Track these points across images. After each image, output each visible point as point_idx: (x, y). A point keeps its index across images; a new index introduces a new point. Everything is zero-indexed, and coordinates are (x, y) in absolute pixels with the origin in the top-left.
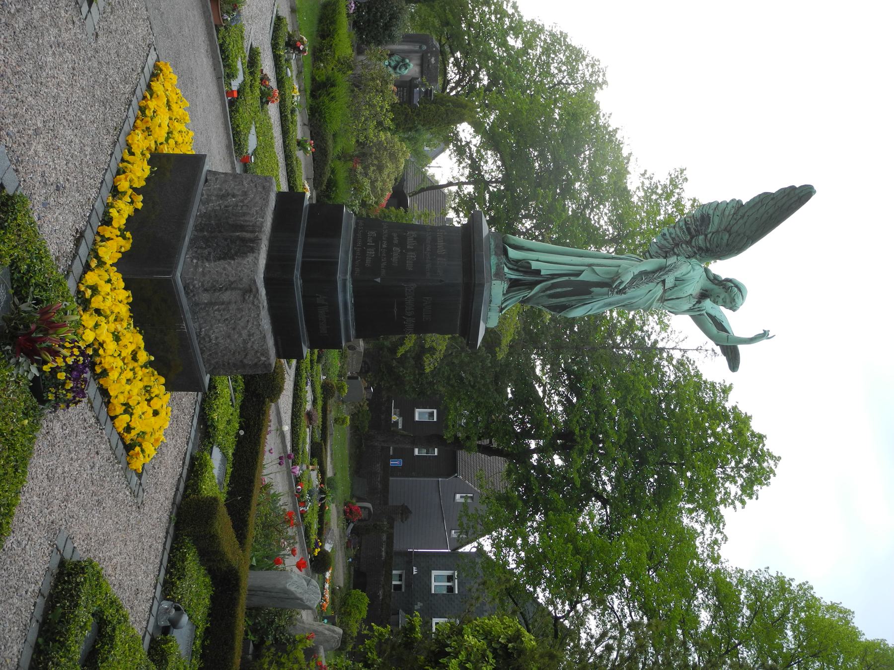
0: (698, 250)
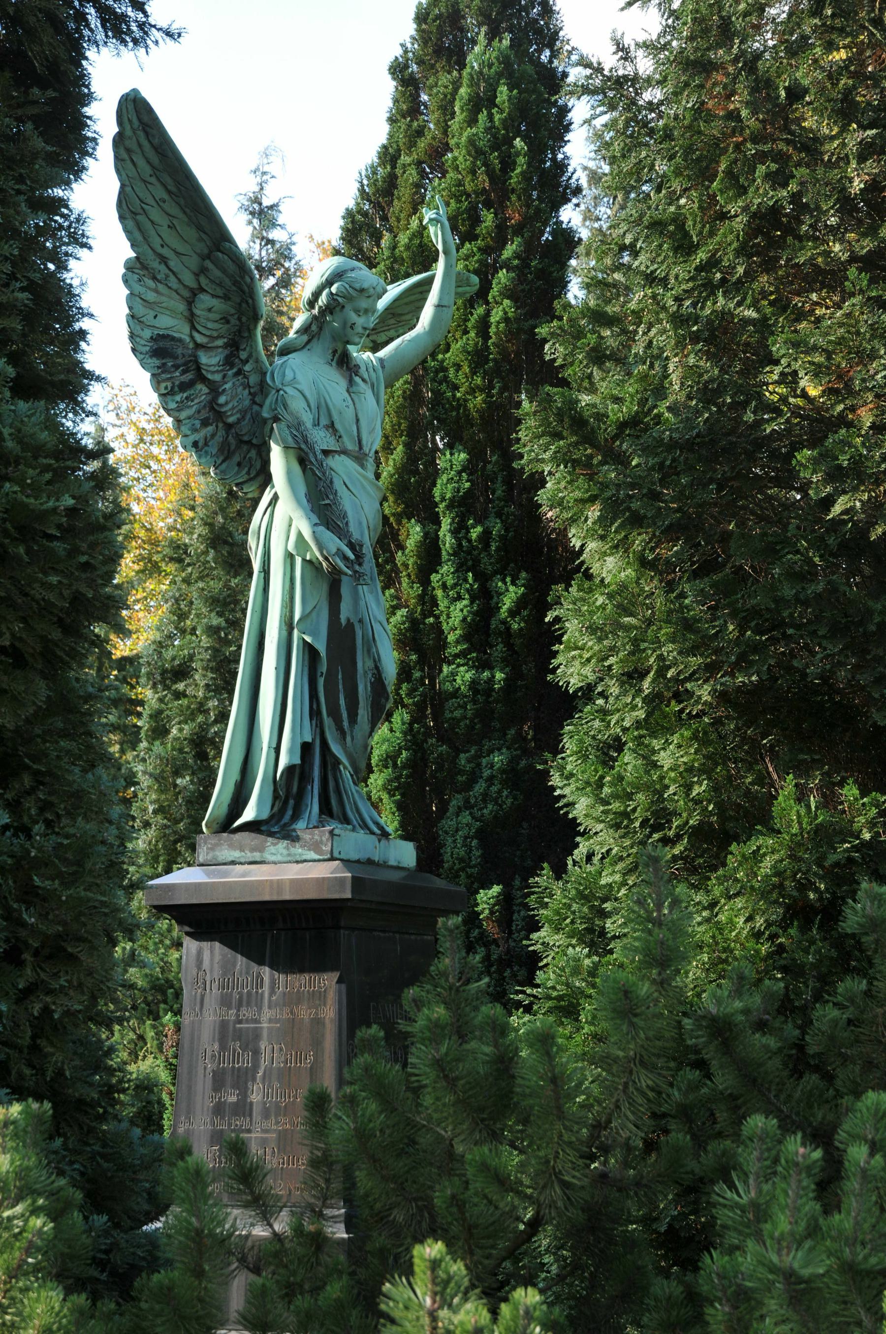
0: (232, 366)
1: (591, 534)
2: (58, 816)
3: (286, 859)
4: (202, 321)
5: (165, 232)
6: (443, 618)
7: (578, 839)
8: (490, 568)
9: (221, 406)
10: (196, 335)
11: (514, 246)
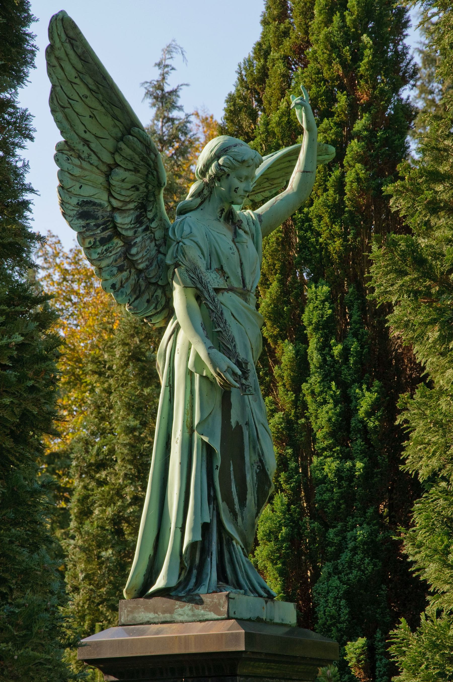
0: (141, 223)
1: (431, 351)
2: (11, 590)
3: (190, 619)
4: (117, 189)
5: (87, 121)
6: (312, 419)
7: (428, 598)
8: (349, 378)
9: (133, 255)
10: (112, 200)
11: (363, 121)
